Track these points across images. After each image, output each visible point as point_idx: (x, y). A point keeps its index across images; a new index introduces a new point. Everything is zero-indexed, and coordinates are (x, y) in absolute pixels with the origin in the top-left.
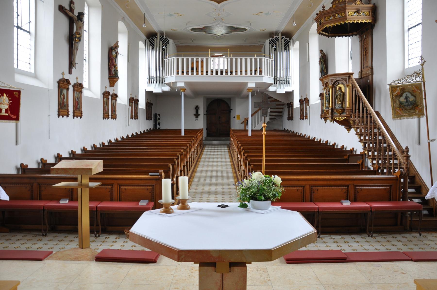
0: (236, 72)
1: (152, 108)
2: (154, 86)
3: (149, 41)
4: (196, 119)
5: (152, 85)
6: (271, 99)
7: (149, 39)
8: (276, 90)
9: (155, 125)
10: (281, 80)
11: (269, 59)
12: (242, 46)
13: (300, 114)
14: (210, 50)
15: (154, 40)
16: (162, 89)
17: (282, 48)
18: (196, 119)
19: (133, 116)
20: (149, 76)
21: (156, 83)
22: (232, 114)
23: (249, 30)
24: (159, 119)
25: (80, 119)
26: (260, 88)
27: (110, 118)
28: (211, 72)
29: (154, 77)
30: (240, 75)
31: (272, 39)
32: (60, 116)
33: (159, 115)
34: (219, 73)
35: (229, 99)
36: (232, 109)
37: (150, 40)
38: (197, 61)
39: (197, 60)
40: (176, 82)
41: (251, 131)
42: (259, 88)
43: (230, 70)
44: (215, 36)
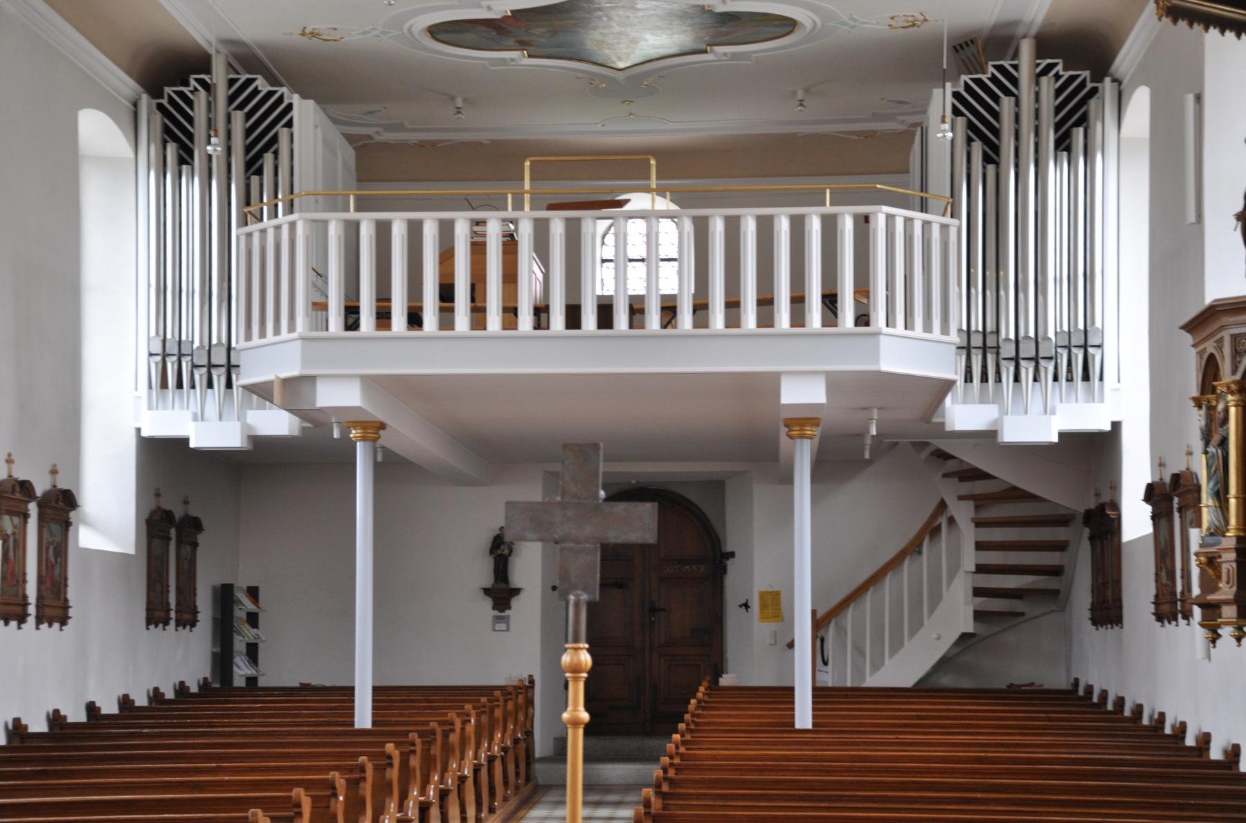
0: (733, 305)
1: (200, 552)
2: (195, 406)
3: (161, 107)
4: (498, 619)
5: (181, 396)
6: (979, 487)
7: (162, 97)
8: (996, 422)
9: (222, 661)
10: (1033, 354)
11: (918, 217)
12: (795, 134)
13: (1157, 581)
14: (527, 164)
15: (190, 103)
16: (245, 426)
17: (1037, 145)
18: (498, 619)
19: (168, 610)
20: (164, 341)
21: (210, 385)
22: (732, 582)
23: (814, 22)
24: (253, 619)
25: (61, 630)
26: (880, 409)
27: (31, 620)
28: (663, 309)
29: (197, 344)
30: (823, 326)
31: (973, 80)
32: (42, 623)
33: (253, 593)
34: (654, 319)
35: (716, 486)
36: (732, 555)
37: (165, 102)
38: (477, 239)
39: (474, 233)
40: (310, 380)
41: (814, 696)
42: (875, 414)
43: (346, 301)
44: (603, 78)
